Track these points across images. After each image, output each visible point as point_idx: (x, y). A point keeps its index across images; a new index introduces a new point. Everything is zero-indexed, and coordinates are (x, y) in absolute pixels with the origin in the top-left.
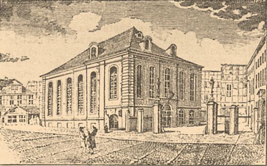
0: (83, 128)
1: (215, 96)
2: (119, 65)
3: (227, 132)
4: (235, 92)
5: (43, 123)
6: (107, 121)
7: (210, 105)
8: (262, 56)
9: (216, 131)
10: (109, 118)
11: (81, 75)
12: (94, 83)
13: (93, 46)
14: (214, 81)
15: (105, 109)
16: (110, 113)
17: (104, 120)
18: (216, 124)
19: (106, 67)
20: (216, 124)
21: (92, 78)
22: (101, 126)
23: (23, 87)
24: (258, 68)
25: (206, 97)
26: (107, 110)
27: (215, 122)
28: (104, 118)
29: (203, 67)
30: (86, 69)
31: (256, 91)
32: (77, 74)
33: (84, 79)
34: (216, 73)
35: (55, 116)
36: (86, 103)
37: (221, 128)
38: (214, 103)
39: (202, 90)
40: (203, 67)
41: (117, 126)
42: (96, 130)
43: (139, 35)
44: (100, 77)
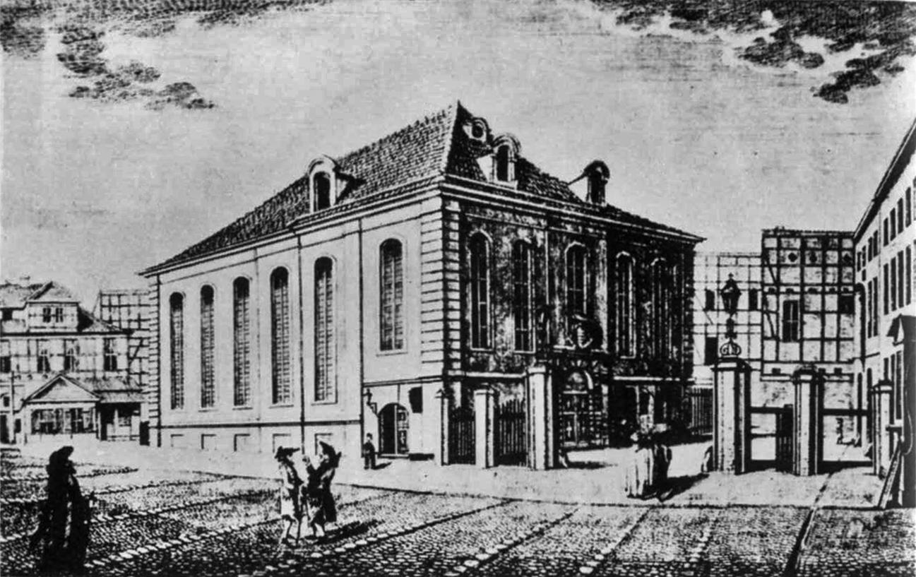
0: (290, 451)
1: (741, 341)
2: (409, 237)
3: (784, 462)
4: (812, 327)
5: (153, 434)
6: (372, 425)
7: (723, 370)
8: (897, 208)
9: (746, 465)
10: (379, 416)
11: (601, 164)
12: (208, 476)
13: (318, 169)
14: (740, 286)
15: (363, 385)
16: (383, 397)
17: (361, 422)
18: (745, 436)
19: (568, 181)
20: (745, 436)
21: (318, 277)
22: (349, 445)
23: (79, 310)
24: (891, 243)
25: (711, 344)
26: (372, 390)
27: (742, 426)
28: (362, 416)
29: (701, 240)
30: (300, 247)
31: (885, 324)
32: (267, 267)
33: (293, 279)
34: (742, 261)
35: (191, 410)
36: (299, 375)
37: (764, 449)
38: (740, 362)
39: (695, 321)
40: (701, 240)
41: (403, 447)
42: (332, 458)
43: (477, 131)
44: (345, 274)
